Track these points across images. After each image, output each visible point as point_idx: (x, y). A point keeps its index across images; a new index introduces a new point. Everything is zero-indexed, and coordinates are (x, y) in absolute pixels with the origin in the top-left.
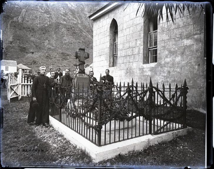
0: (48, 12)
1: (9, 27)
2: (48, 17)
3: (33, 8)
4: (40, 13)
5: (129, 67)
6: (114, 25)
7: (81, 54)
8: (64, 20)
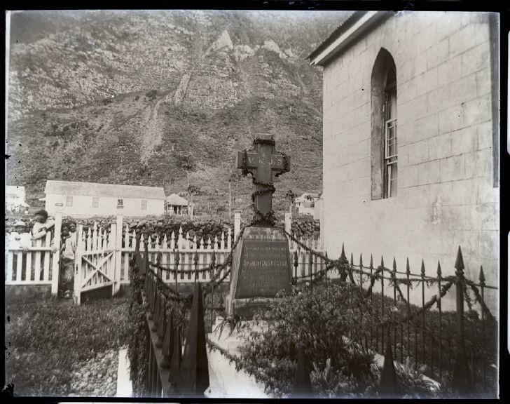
0: (235, 75)
1: (155, 116)
2: (235, 88)
3: (203, 71)
4: (217, 80)
5: (439, 201)
6: (385, 69)
7: (264, 161)
8: (271, 91)
